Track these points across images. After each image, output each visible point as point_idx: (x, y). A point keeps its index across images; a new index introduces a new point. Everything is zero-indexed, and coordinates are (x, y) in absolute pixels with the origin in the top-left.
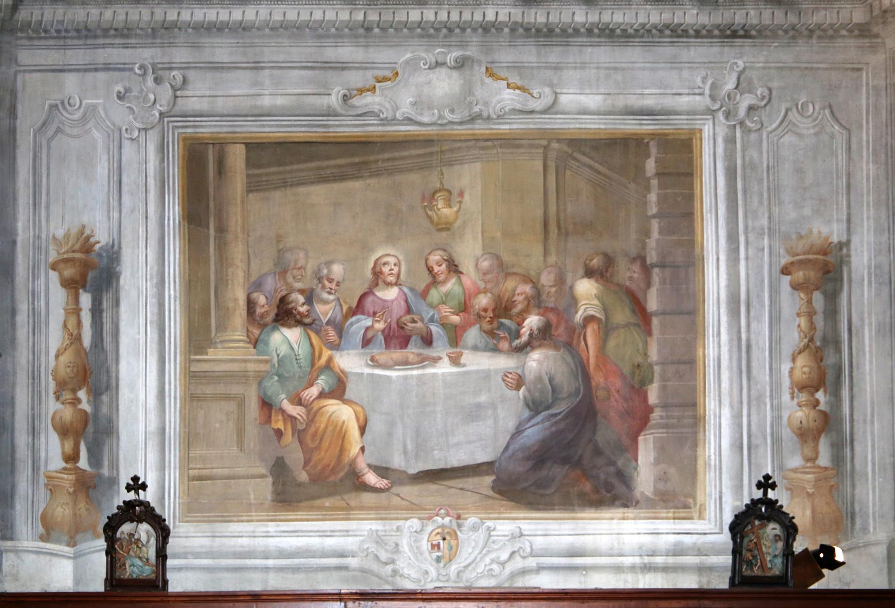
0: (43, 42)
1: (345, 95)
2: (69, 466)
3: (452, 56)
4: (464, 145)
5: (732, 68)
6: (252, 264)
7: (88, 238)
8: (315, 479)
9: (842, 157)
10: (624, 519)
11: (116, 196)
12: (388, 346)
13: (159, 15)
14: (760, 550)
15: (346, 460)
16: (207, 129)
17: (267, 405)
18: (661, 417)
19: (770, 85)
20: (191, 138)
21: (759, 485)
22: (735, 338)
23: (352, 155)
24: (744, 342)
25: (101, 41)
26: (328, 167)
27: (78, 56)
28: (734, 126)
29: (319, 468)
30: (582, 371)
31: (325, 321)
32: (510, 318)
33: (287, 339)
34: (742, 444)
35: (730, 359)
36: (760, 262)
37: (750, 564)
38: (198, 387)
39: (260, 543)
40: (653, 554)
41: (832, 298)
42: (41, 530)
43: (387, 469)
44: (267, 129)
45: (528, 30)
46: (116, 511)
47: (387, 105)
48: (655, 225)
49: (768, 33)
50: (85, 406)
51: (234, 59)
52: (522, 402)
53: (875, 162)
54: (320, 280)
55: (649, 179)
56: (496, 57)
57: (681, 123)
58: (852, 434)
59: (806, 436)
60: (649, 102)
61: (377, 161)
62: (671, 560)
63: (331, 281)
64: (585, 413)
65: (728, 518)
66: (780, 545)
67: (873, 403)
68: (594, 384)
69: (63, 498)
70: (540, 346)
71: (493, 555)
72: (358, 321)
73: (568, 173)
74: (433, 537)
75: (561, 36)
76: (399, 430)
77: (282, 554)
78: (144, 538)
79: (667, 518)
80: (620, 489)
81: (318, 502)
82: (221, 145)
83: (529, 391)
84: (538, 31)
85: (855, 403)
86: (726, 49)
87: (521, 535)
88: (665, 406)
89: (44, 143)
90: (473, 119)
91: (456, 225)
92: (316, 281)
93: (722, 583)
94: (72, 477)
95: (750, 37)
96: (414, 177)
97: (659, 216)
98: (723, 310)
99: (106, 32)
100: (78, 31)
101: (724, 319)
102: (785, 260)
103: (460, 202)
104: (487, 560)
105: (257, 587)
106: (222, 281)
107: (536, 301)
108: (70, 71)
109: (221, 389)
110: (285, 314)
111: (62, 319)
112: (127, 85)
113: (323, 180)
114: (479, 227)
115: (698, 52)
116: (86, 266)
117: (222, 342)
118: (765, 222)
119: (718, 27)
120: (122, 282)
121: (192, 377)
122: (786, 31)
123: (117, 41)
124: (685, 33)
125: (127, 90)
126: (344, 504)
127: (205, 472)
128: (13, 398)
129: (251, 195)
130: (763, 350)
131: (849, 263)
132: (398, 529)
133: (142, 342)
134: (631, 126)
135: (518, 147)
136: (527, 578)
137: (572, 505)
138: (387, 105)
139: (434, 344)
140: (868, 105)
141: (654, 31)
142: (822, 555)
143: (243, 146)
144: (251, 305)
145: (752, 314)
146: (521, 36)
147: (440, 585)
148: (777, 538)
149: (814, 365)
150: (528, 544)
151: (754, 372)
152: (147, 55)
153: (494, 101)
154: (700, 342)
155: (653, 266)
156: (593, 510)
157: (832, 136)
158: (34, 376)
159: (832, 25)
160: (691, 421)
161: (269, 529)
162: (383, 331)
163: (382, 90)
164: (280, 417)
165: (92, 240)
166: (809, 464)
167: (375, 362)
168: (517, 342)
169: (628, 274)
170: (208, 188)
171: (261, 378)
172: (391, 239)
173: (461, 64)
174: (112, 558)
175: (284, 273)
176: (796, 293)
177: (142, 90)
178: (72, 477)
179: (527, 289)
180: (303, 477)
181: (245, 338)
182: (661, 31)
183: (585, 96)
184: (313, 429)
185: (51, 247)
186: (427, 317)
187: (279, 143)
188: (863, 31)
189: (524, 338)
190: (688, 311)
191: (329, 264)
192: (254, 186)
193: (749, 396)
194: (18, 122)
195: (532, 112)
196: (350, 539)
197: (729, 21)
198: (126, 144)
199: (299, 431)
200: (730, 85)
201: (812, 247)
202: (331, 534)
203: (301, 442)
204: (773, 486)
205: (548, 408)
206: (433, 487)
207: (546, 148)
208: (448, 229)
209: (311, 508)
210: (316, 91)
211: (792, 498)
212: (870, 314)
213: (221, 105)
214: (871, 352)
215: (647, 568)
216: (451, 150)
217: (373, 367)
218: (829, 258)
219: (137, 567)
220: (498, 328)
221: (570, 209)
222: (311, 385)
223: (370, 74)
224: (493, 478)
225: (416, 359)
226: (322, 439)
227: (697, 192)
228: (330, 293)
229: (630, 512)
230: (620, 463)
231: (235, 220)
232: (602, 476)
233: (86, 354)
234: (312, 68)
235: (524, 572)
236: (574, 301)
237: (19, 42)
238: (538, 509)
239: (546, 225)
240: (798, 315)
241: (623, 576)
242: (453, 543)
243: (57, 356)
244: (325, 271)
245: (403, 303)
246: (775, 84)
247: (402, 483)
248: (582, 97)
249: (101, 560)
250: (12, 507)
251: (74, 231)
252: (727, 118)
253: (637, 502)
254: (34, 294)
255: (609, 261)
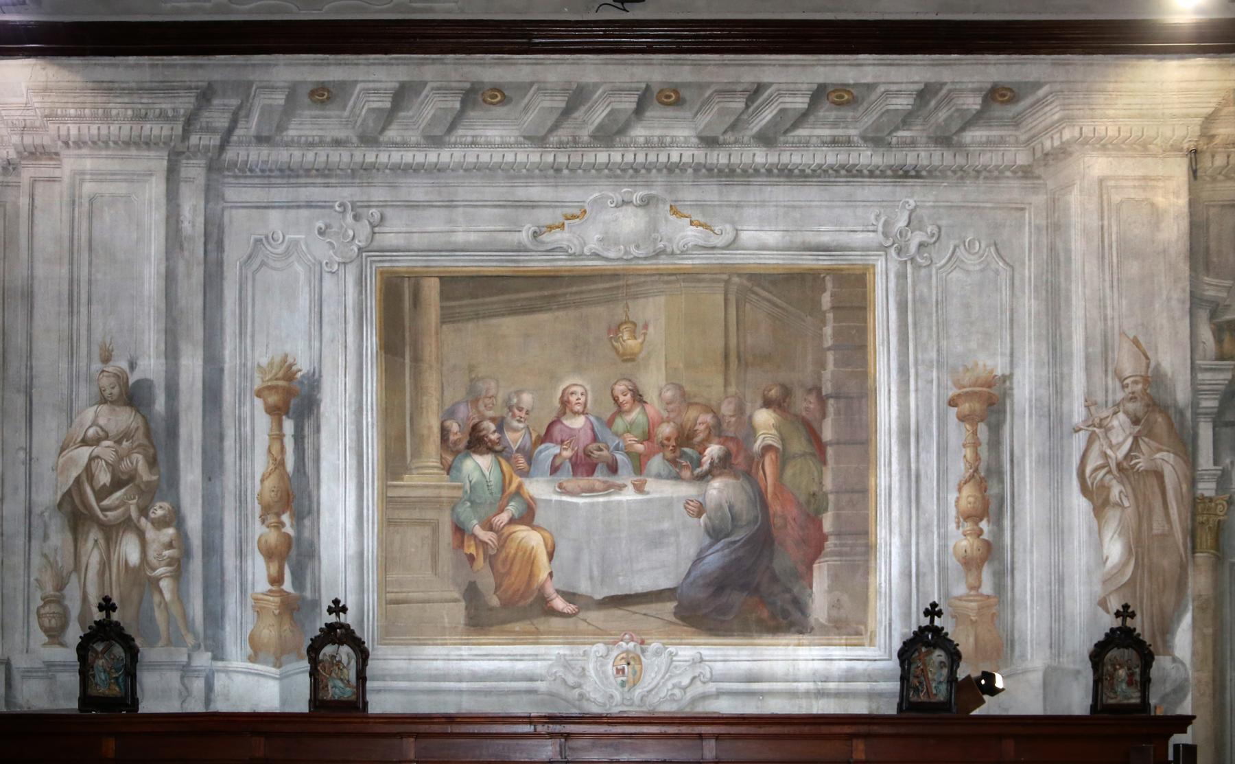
0: (248, 181)
1: (535, 232)
2: (274, 588)
3: (637, 196)
4: (649, 279)
5: (903, 207)
6: (446, 393)
7: (290, 366)
8: (506, 604)
9: (1006, 293)
10: (799, 645)
11: (317, 327)
12: (575, 474)
13: (358, 157)
14: (926, 677)
15: (535, 586)
16: (404, 263)
17: (460, 530)
18: (835, 545)
19: (939, 223)
20: (387, 272)
21: (927, 613)
22: (905, 467)
23: (541, 289)
24: (913, 472)
25: (302, 180)
26: (518, 300)
27: (280, 194)
28: (906, 262)
29: (510, 592)
30: (760, 499)
31: (515, 448)
32: (692, 447)
33: (479, 466)
34: (910, 572)
35: (901, 488)
36: (929, 393)
37: (917, 690)
38: (395, 512)
39: (454, 666)
40: (826, 680)
41: (996, 430)
42: (249, 650)
43: (574, 594)
44: (461, 264)
45: (710, 170)
46: (318, 633)
47: (576, 242)
48: (830, 357)
49: (938, 173)
50: (289, 530)
51: (427, 198)
52: (703, 529)
53: (1036, 298)
54: (510, 408)
55: (825, 312)
56: (680, 196)
57: (856, 258)
58: (1013, 562)
59: (971, 564)
60: (825, 239)
61: (565, 294)
62: (843, 686)
63: (520, 409)
64: (762, 541)
65: (897, 645)
66: (945, 671)
67: (1032, 531)
68: (771, 512)
69: (270, 620)
70: (720, 475)
71: (675, 681)
72: (547, 449)
73: (748, 306)
74: (618, 662)
75: (742, 176)
76: (585, 557)
77: (475, 677)
78: (345, 660)
79: (840, 645)
80: (796, 615)
81: (508, 626)
82: (416, 279)
83: (710, 518)
84: (720, 171)
85: (1017, 533)
86: (898, 189)
87: (702, 661)
88: (838, 534)
89: (250, 275)
90: (657, 254)
91: (641, 356)
92: (506, 410)
93: (891, 710)
94: (277, 599)
95: (921, 177)
96: (601, 310)
97: (834, 348)
98: (894, 440)
99: (308, 172)
100: (281, 170)
101: (895, 449)
102: (953, 392)
103: (645, 334)
104: (670, 685)
105: (451, 710)
106: (417, 409)
107: (717, 431)
108: (273, 207)
109: (416, 514)
110: (477, 442)
111: (266, 444)
112: (328, 221)
113: (514, 312)
114: (663, 356)
115: (871, 191)
116: (289, 393)
117: (417, 468)
118: (934, 355)
119: (891, 167)
120: (322, 409)
121: (389, 503)
122: (954, 172)
123: (319, 180)
124: (860, 173)
125: (328, 226)
126: (533, 629)
127: (401, 596)
128: (222, 520)
129: (444, 327)
130: (931, 481)
131: (1012, 395)
132: (585, 653)
133: (342, 466)
134: (808, 261)
135: (700, 281)
136: (707, 702)
137: (751, 631)
138: (576, 242)
139: (620, 472)
140: (1030, 243)
141: (830, 171)
142: (983, 682)
143: (437, 280)
144: (444, 432)
145: (921, 444)
146: (705, 176)
147: (625, 709)
148: (942, 665)
149: (979, 495)
150: (708, 669)
151: (923, 501)
152: (347, 194)
153: (678, 237)
154: (872, 471)
155: (828, 397)
156: (770, 637)
157: (997, 272)
158: (241, 501)
159: (997, 167)
160: (863, 549)
161: (463, 653)
162: (570, 459)
163: (570, 226)
164: (472, 542)
165: (294, 368)
166: (973, 593)
167: (563, 490)
168: (698, 471)
169: (805, 404)
170: (403, 319)
171: (454, 505)
172: (578, 369)
173: (646, 203)
174: (315, 679)
175: (475, 401)
176: (962, 424)
177: (342, 226)
178: (277, 599)
179: (708, 418)
180: (495, 601)
181: (439, 465)
182: (837, 171)
183: (763, 232)
184: (503, 555)
185: (256, 375)
186: (612, 445)
187: (472, 277)
188: (1026, 173)
189: (706, 467)
190: (860, 441)
191: (518, 393)
192: (448, 317)
193: (918, 524)
194: (225, 255)
195: (713, 248)
196: (539, 663)
197: (902, 162)
198: (326, 276)
199: (491, 556)
200: (902, 223)
201: (977, 379)
202: (522, 657)
203: (492, 567)
204: (939, 614)
205: (727, 535)
206: (618, 613)
207: (727, 282)
208: (633, 360)
209: (502, 632)
210: (508, 228)
211: (957, 625)
212: (1030, 445)
213: (417, 241)
214: (1031, 482)
215: (821, 694)
216: (636, 284)
217: (561, 494)
218: (992, 391)
219: (338, 689)
220: (681, 457)
221: (749, 340)
222: (502, 511)
223: (559, 212)
224: (675, 604)
225: (602, 486)
226: (512, 564)
227: (870, 325)
228: (519, 421)
229: (805, 639)
230: (796, 590)
231: (430, 350)
232: (779, 603)
233: (289, 479)
234: (504, 206)
235: (705, 697)
236: (752, 431)
237: (226, 180)
238: (717, 635)
239: (726, 356)
240: (964, 446)
241: (797, 701)
242: (637, 667)
243: (262, 481)
244: (515, 400)
245: (589, 432)
246: (943, 223)
247: (588, 608)
248: (761, 234)
249: (304, 681)
250: (223, 628)
251: (278, 360)
252: (899, 254)
253: (812, 629)
254: (240, 421)
255: (787, 392)
